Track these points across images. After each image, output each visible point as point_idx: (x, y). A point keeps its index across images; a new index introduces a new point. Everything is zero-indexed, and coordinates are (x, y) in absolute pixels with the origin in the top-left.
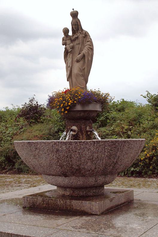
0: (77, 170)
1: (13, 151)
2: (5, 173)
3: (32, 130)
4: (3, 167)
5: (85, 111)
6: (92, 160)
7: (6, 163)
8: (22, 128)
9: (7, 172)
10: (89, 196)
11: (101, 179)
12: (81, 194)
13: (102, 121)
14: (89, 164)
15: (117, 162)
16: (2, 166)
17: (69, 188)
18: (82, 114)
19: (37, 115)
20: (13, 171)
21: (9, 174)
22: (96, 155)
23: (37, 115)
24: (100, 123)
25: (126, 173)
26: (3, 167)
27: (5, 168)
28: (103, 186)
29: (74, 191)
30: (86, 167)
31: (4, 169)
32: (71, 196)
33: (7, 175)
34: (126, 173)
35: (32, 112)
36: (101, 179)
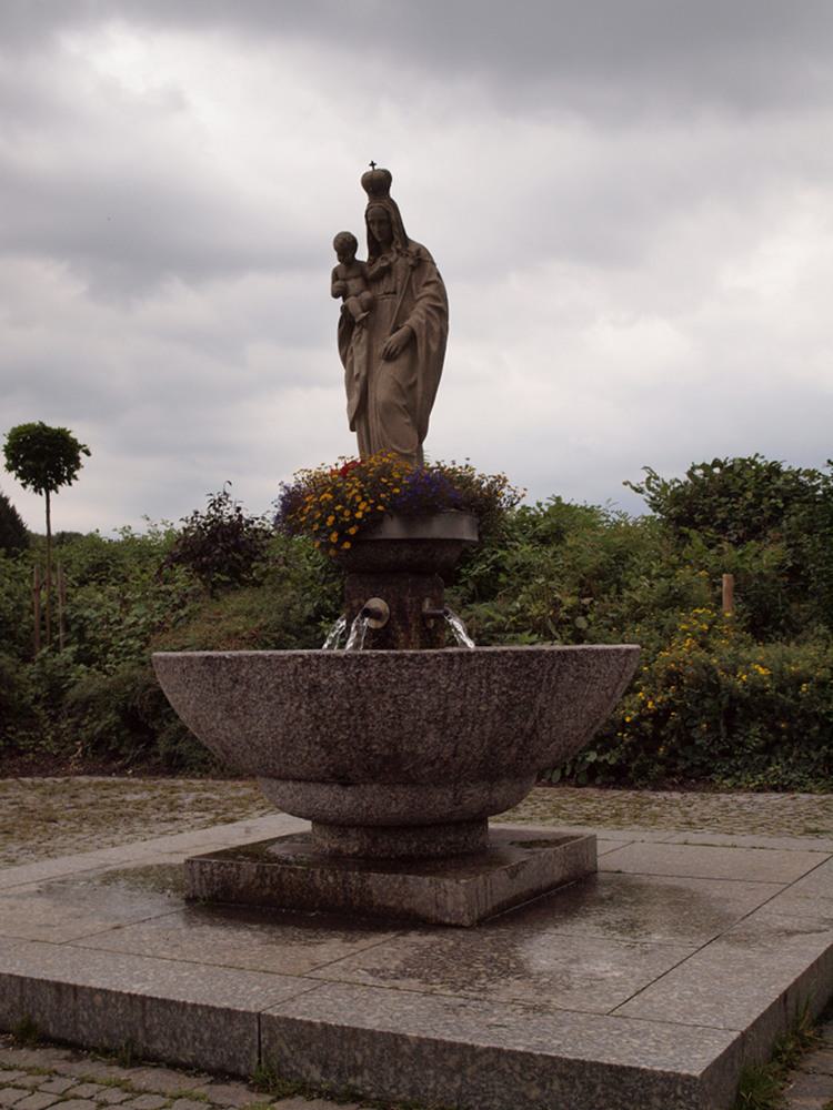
1: (150, 690)
2: (121, 772)
3: (219, 614)
4: (111, 748)
7: (122, 733)
9: (126, 767)
12: (403, 848)
15: (534, 730)
16: (109, 743)
18: (406, 553)
19: (238, 556)
21: (133, 775)
23: (238, 556)
25: (568, 773)
26: (111, 748)
27: (121, 752)
31: (115, 755)
34: (568, 773)
36: (475, 795)
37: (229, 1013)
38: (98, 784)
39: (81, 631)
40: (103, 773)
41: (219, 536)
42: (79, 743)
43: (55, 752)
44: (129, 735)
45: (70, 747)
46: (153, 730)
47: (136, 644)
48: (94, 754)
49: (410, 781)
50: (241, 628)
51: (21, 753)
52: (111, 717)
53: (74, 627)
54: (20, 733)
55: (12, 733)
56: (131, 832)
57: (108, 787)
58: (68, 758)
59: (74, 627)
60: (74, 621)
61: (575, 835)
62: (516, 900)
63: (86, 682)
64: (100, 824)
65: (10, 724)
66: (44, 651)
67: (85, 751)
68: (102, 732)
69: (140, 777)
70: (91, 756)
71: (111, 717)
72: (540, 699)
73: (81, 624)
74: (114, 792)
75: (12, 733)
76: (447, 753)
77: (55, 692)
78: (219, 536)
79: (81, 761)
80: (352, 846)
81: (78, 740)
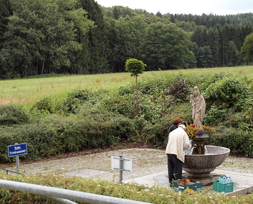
0: (194, 167)
1: (162, 130)
2: (156, 148)
3: (178, 111)
4: (154, 142)
5: (200, 138)
6: (200, 163)
7: (157, 139)
8: (169, 106)
9: (157, 146)
10: (202, 177)
11: (206, 170)
12: (198, 176)
13: (238, 107)
14: (199, 164)
15: (212, 163)
16: (153, 141)
17: (192, 173)
18: (199, 139)
19: (183, 93)
20: (162, 146)
21: (159, 149)
22: (202, 161)
23: (183, 93)
24: (236, 108)
25: (250, 155)
26: (154, 142)
27: (156, 143)
28: (209, 173)
29: (194, 175)
30: (198, 166)
31: (155, 144)
32: (193, 177)
33: (158, 150)
34: (250, 155)
35: (179, 91)
36: (206, 170)
37: (103, 73)
38: (152, 151)
39: (145, 110)
40: (152, 148)
41: (178, 89)
42: (146, 140)
43: (141, 142)
44: (158, 139)
45: (144, 141)
46: (163, 138)
47: (158, 116)
48: (150, 143)
49: (198, 169)
50: (183, 116)
51: (133, 142)
52: (154, 135)
53: (143, 110)
54: (133, 137)
55: (131, 137)
56: (162, 167)
57: (155, 152)
58: (144, 143)
59: (143, 110)
60: (143, 108)
61: (218, 175)
62: (210, 183)
63: (148, 126)
64: (156, 164)
65: (130, 135)
66: (137, 116)
67: (148, 142)
68: (151, 138)
69: (161, 149)
70: (149, 143)
71: (154, 135)
72: (212, 160)
73: (145, 109)
74: (155, 154)
75: (131, 137)
76: (201, 166)
77: (140, 126)
78: (178, 89)
79: (147, 144)
80: (192, 175)
81: (146, 139)
